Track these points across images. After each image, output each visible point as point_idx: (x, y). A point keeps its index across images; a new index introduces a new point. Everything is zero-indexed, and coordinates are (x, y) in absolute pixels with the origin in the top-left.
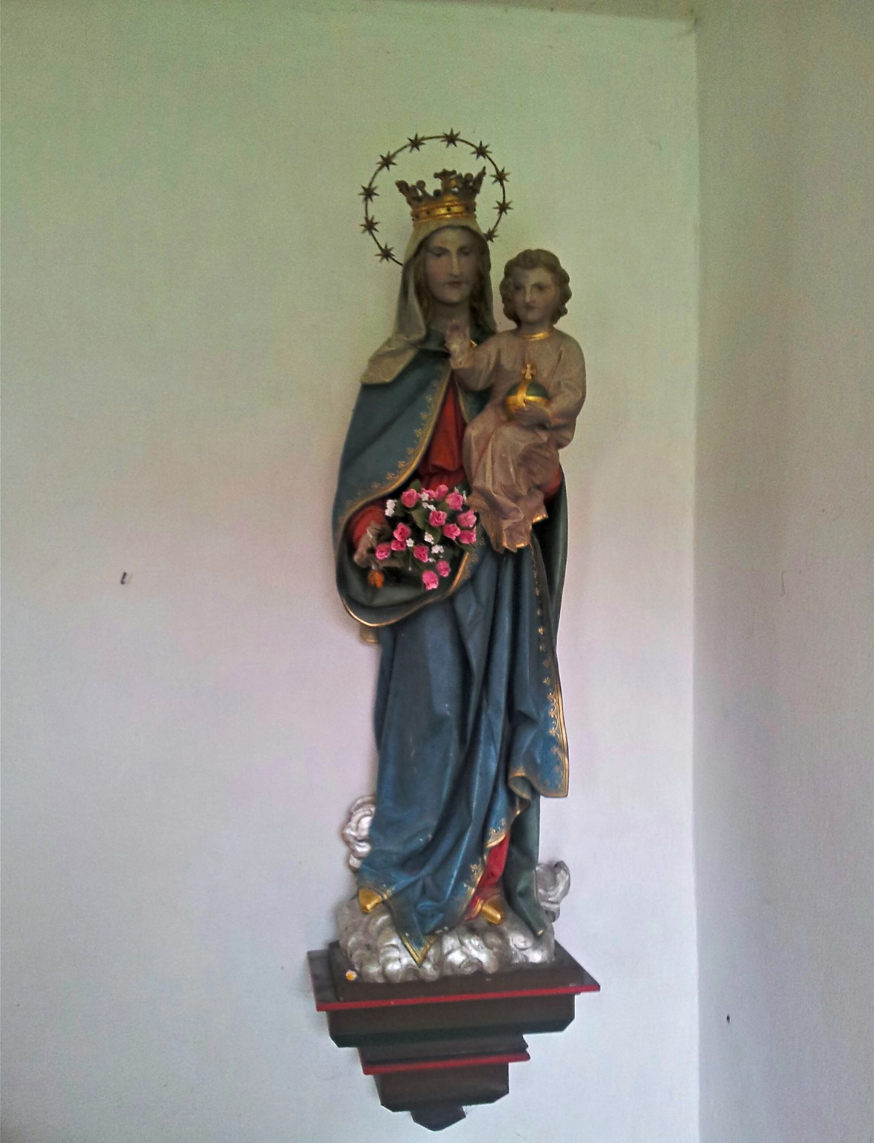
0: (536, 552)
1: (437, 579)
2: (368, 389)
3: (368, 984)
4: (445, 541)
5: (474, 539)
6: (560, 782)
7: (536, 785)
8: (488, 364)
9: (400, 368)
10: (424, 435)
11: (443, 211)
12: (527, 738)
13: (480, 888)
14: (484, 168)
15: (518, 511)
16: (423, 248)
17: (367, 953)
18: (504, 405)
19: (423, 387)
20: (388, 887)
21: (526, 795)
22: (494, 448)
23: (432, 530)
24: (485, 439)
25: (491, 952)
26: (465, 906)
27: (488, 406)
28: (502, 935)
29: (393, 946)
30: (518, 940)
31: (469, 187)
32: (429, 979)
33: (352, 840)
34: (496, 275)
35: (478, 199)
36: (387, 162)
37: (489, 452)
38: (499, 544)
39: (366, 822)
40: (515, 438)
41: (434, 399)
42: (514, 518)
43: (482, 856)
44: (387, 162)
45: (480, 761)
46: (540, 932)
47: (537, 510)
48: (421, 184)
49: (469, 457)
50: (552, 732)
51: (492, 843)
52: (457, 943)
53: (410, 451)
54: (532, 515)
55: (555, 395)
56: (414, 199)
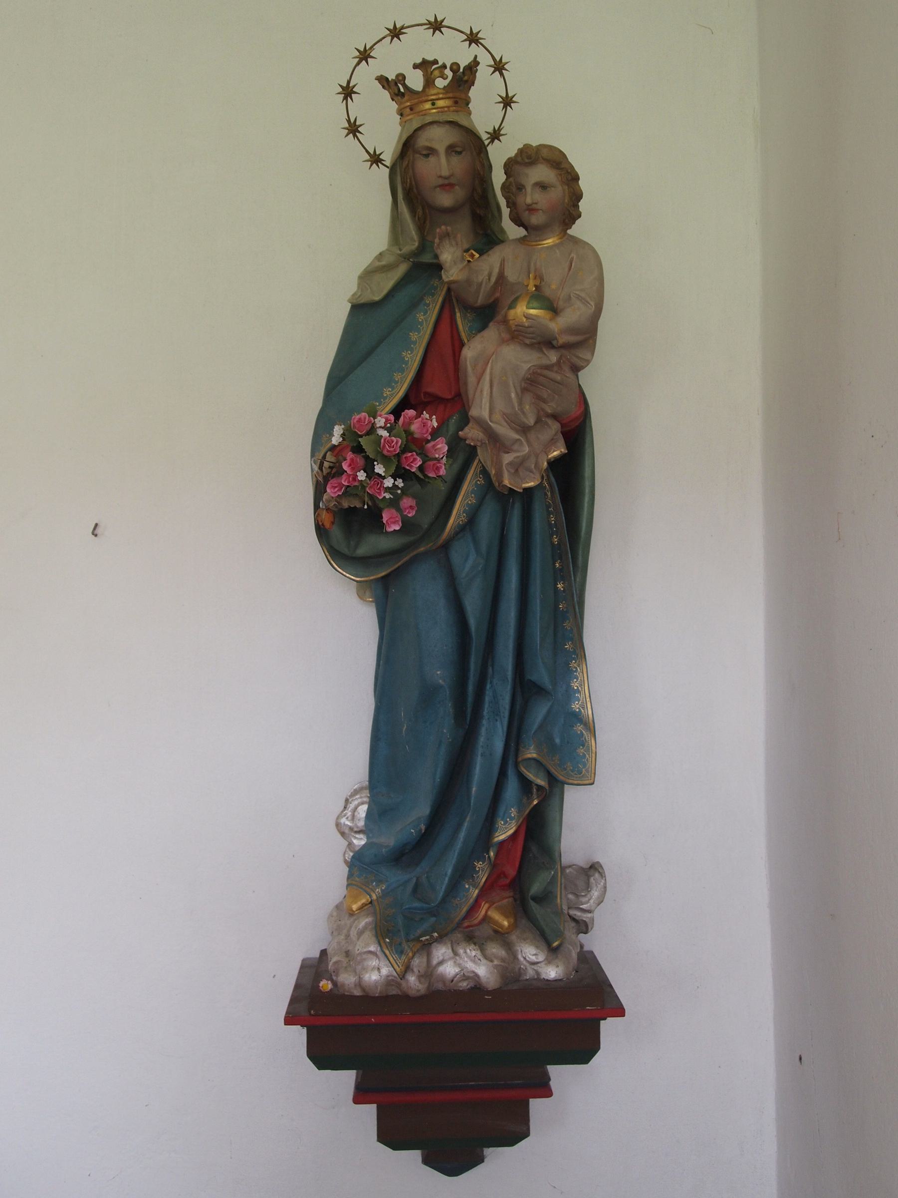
0: (552, 493)
1: (399, 518)
2: (358, 309)
3: (343, 996)
4: (399, 473)
5: (443, 472)
6: (585, 765)
7: (553, 770)
8: (490, 275)
9: (390, 284)
10: (413, 359)
11: (428, 105)
12: (539, 712)
13: (485, 891)
14: (476, 57)
15: (521, 443)
16: (407, 147)
17: (345, 961)
18: (505, 321)
19: (415, 304)
20: (377, 886)
21: (541, 782)
22: (493, 369)
23: (386, 460)
24: (485, 360)
25: (491, 964)
26: (465, 910)
27: (491, 324)
28: (509, 946)
29: (370, 952)
30: (529, 953)
31: (464, 78)
32: (412, 993)
33: (347, 831)
34: (498, 178)
35: (473, 93)
36: (365, 56)
37: (487, 377)
38: (500, 482)
39: (363, 810)
40: (519, 359)
41: (426, 319)
42: (518, 451)
43: (488, 853)
44: (365, 56)
45: (482, 740)
46: (555, 944)
47: (552, 442)
48: (401, 78)
49: (466, 384)
50: (575, 706)
51: (501, 836)
52: (449, 952)
53: (397, 376)
54: (547, 448)
55: (562, 310)
56: (397, 95)
